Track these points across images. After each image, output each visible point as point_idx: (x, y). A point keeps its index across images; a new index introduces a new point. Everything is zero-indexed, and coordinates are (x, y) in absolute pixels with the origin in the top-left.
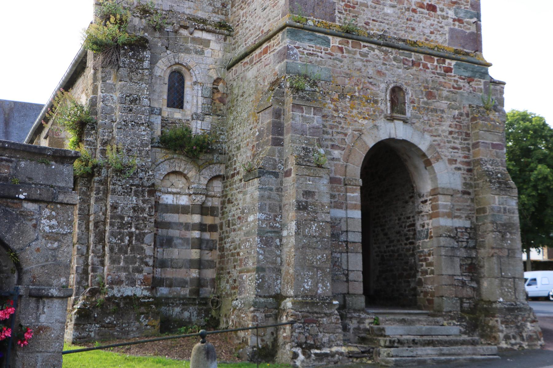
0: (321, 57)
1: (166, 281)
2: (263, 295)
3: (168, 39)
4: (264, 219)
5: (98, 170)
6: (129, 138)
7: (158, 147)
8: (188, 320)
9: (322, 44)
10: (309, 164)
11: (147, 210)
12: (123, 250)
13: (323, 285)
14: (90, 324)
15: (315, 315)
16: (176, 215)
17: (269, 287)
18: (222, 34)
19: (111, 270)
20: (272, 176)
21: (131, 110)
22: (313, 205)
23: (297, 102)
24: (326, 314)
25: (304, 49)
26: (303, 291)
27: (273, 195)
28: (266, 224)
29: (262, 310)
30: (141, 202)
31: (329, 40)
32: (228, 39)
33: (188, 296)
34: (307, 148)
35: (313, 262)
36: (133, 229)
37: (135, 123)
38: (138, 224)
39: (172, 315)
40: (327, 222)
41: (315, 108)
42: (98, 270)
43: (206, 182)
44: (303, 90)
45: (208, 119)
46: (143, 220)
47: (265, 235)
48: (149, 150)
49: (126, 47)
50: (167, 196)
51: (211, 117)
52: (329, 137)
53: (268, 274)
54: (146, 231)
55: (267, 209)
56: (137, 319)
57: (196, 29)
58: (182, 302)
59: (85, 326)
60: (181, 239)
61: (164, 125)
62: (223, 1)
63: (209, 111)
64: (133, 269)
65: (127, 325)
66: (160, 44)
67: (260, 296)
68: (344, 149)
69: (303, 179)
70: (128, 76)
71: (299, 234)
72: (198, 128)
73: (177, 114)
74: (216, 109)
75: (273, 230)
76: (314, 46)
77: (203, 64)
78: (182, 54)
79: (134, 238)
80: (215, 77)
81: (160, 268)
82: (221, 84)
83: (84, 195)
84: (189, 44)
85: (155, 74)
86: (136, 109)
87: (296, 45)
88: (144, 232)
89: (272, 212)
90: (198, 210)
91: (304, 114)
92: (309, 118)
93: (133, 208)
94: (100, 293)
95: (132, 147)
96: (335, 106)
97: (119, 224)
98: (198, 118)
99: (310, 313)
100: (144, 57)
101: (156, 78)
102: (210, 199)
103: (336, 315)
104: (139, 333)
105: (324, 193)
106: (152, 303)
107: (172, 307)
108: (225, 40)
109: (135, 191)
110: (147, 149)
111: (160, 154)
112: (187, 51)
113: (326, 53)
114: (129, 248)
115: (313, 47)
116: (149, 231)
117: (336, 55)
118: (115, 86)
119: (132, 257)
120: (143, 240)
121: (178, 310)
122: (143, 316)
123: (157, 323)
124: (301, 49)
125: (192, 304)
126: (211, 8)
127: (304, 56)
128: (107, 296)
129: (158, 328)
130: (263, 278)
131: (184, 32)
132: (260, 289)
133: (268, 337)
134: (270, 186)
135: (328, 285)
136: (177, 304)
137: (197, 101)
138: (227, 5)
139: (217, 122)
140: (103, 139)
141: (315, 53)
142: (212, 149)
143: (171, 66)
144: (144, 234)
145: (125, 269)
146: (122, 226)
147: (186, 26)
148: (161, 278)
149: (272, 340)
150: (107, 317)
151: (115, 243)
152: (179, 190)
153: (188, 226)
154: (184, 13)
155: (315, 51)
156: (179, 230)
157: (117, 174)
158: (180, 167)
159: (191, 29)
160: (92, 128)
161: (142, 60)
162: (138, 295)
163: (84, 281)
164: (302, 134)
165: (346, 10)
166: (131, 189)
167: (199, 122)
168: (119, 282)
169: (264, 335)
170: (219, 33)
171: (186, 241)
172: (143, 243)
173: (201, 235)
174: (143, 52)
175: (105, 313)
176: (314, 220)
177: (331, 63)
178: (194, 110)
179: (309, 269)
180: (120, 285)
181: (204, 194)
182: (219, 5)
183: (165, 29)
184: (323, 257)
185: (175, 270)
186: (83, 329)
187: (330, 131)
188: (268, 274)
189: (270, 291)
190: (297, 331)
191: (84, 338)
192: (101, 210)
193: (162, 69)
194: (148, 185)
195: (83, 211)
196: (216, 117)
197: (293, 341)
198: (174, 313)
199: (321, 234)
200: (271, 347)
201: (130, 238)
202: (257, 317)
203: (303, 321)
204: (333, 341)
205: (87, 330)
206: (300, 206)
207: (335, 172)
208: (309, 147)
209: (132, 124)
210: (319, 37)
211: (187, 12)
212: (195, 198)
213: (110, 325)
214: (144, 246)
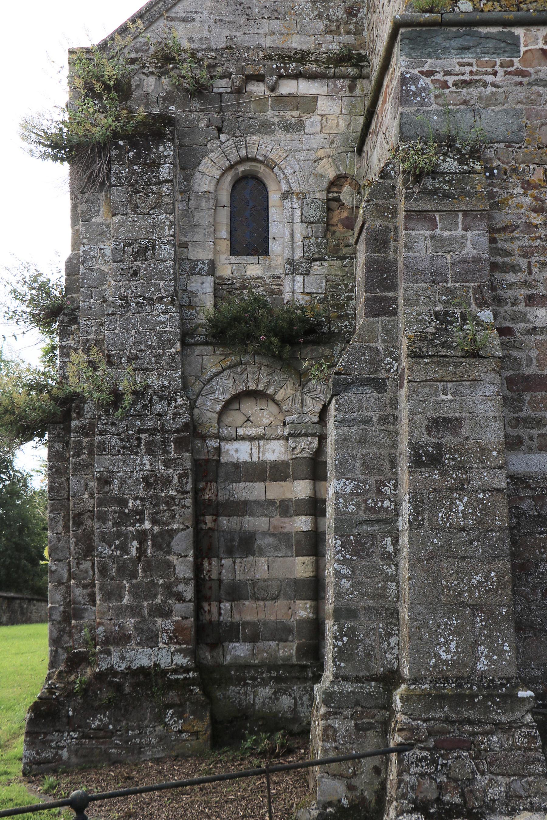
0: (494, 85)
1: (244, 629)
2: (354, 674)
3: (221, 110)
4: (352, 493)
5: (78, 407)
6: (133, 332)
7: (206, 343)
8: (289, 715)
9: (496, 51)
10: (443, 352)
11: (175, 481)
12: (126, 571)
13: (491, 649)
14: (58, 731)
15: (467, 727)
16: (259, 486)
17: (368, 655)
18: (344, 77)
19: (104, 613)
20: (368, 390)
21: (135, 274)
22: (456, 450)
23: (415, 206)
24: (498, 725)
25: (447, 73)
26: (435, 666)
27: (372, 433)
28: (357, 505)
29: (348, 712)
30: (160, 465)
31: (518, 38)
32: (358, 87)
33: (294, 660)
34: (446, 314)
35: (460, 594)
36: (147, 525)
37: (145, 298)
38: (157, 513)
39: (254, 705)
40: (498, 490)
41: (466, 213)
42: (86, 615)
44: (434, 173)
45: (318, 269)
46: (167, 504)
47: (355, 531)
48: (177, 353)
49: (121, 143)
50: (236, 445)
51: (325, 264)
52: (521, 276)
53: (363, 623)
54: (175, 526)
55: (358, 466)
56: (160, 718)
57: (281, 77)
58: (274, 674)
59: (49, 737)
60: (274, 535)
62: (348, 4)
63: (319, 252)
64: (150, 610)
65: (137, 732)
66: (202, 125)
67: (345, 679)
69: (426, 390)
70: (129, 202)
71: (420, 526)
72: (297, 290)
73: (254, 268)
74: (338, 245)
75: (374, 516)
76: (473, 61)
77: (303, 150)
78: (255, 138)
79: (149, 543)
80: (331, 174)
81: (228, 601)
82: (346, 188)
83: (58, 460)
84: (270, 113)
85: (196, 188)
86: (146, 270)
87: (426, 68)
88: (172, 530)
89: (371, 474)
90: (305, 469)
91: (438, 232)
92: (454, 240)
93: (146, 479)
94: (89, 664)
95: (140, 351)
96: (536, 198)
97: (116, 515)
99: (452, 723)
100: (160, 157)
101: (199, 197)
103: (528, 726)
104: (163, 750)
105: (486, 418)
106: (193, 681)
107: (253, 686)
108: (352, 88)
109: (148, 444)
110: (173, 350)
111: (210, 360)
112: (266, 128)
113: (506, 73)
114: (140, 565)
115: (470, 65)
116: (181, 527)
117: (537, 73)
118: (108, 226)
119: (147, 583)
120: (169, 545)
121: (265, 692)
122: (171, 711)
123: (202, 726)
124: (439, 76)
125: (298, 678)
126: (320, 25)
127: (446, 91)
128: (98, 670)
129: (205, 737)
130: (351, 633)
131: (258, 89)
132: (345, 661)
133: (364, 778)
134: (365, 413)
135: (506, 648)
136: (263, 679)
137: (292, 234)
138: (359, 11)
139: (339, 273)
140: (88, 340)
141: (477, 77)
142: (330, 332)
143: (231, 167)
144: (172, 533)
145: (134, 610)
146: (123, 519)
147: (259, 75)
148: (232, 623)
149: (377, 787)
150: (94, 716)
151: (110, 557)
152: (261, 431)
153: (288, 507)
154: (259, 47)
155: (478, 73)
156: (266, 516)
157: (107, 411)
158: (258, 381)
159: (271, 80)
160: (70, 320)
161: (155, 165)
162: (163, 666)
163: (66, 638)
164: (434, 282)
166: (139, 439)
167: (299, 278)
168: (123, 639)
169: (354, 774)
170: (335, 77)
171: (284, 538)
172: (169, 553)
174: (157, 147)
175: (90, 707)
176: (461, 487)
177: (522, 96)
178: (287, 254)
179: (452, 611)
180: (125, 645)
181: (313, 435)
182: (340, 13)
183: (215, 90)
184: (487, 577)
185: (261, 603)
186: (45, 744)
187: (523, 263)
188: (363, 623)
189: (371, 664)
190: (414, 769)
191: (47, 761)
192: (86, 489)
193: (209, 174)
194: (175, 427)
195: (58, 492)
196: (338, 263)
197: (404, 796)
198: (259, 701)
199: (480, 522)
200: (373, 804)
201: (140, 543)
202: (335, 731)
203: (432, 743)
204: (520, 797)
205: (53, 744)
206: (420, 456)
207: (538, 361)
208: (452, 310)
209: (139, 303)
210: (488, 37)
211: (267, 43)
212: (293, 445)
213: (101, 734)
214: (173, 558)
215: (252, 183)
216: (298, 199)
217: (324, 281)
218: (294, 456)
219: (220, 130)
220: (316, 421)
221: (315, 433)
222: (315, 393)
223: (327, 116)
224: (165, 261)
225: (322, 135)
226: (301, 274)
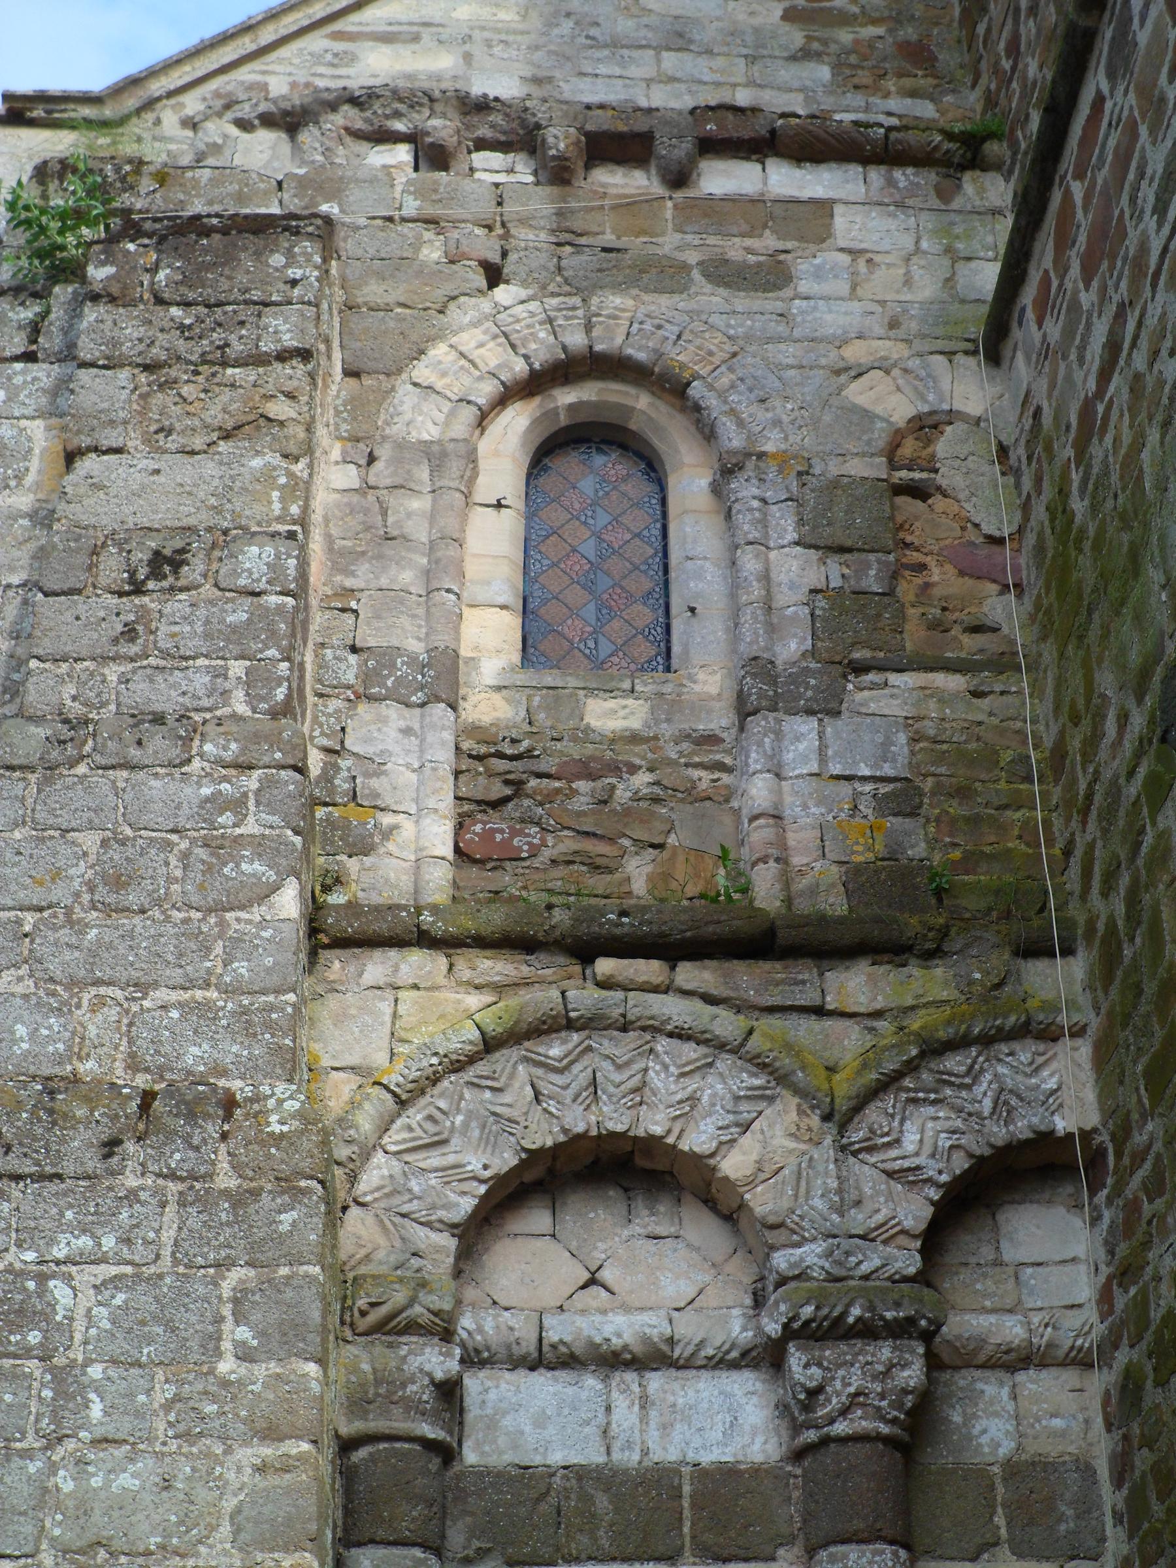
43: (915, 1211)
102: (993, 1389)
217: (902, 738)
218: (811, 1436)
219: (494, 275)
220: (912, 1270)
221: (911, 1321)
222: (893, 1153)
223: (869, 255)
224: (220, 304)
226: (810, 712)
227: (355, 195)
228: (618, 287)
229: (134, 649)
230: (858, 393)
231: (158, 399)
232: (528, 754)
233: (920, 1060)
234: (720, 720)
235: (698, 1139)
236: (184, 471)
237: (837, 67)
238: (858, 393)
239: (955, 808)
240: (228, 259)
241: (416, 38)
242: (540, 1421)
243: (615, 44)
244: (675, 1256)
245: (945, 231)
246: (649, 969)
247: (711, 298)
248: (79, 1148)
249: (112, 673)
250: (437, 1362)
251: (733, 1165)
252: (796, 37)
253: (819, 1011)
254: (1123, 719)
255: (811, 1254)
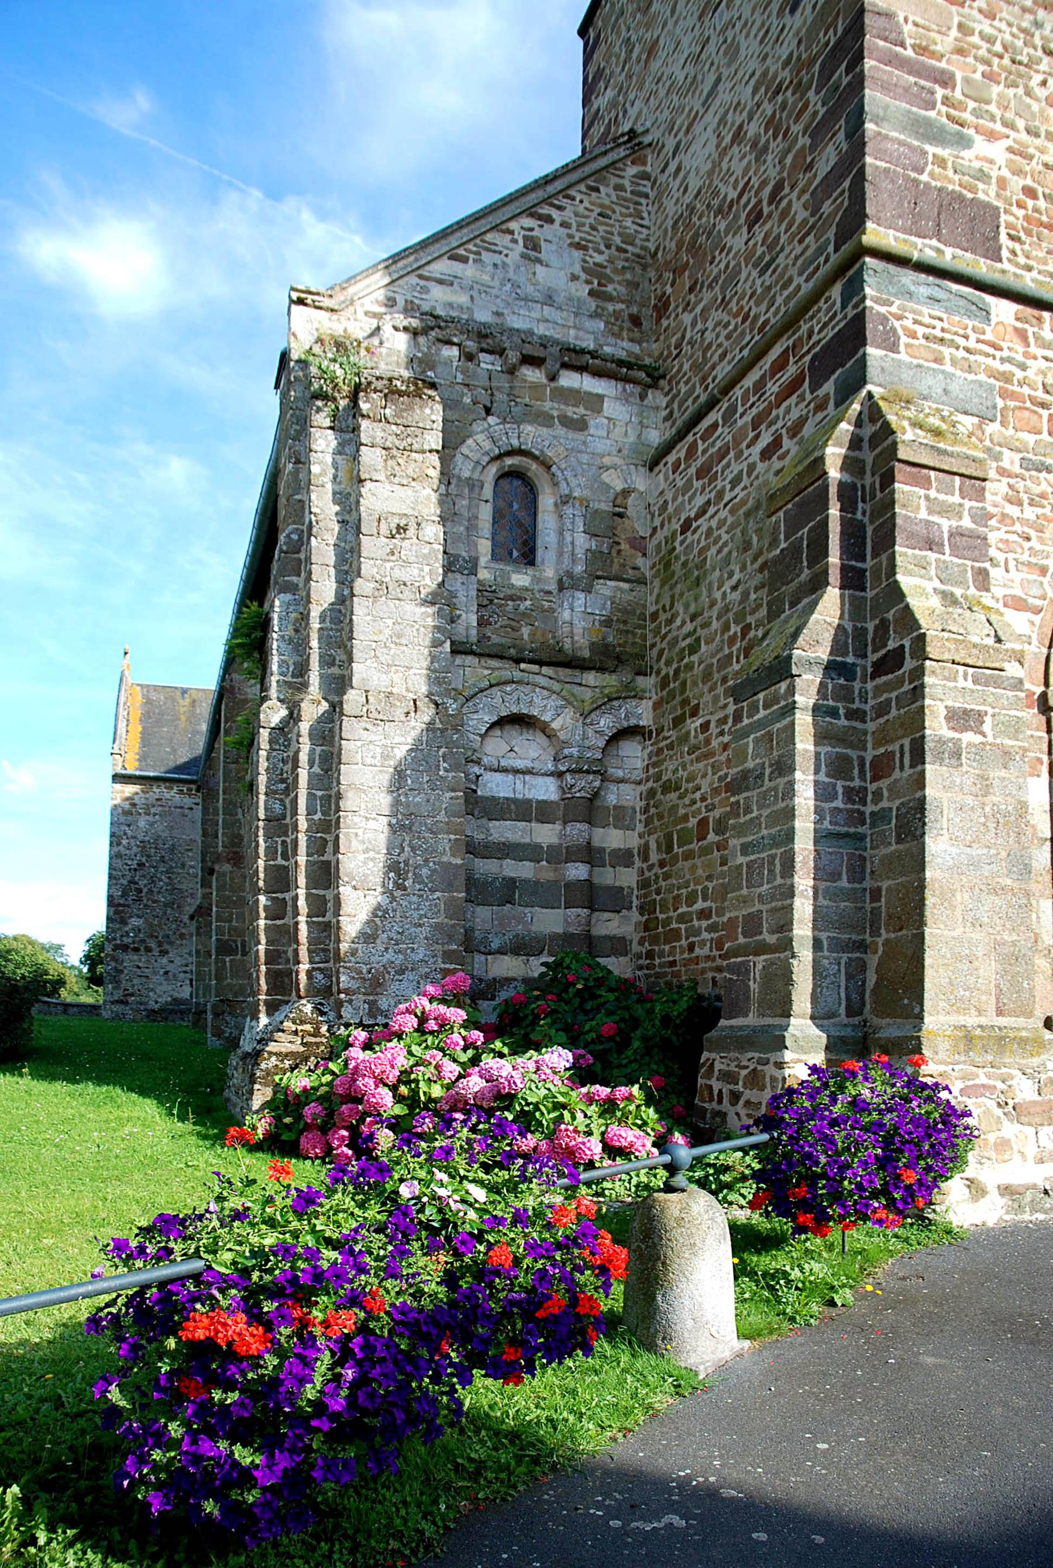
32: (650, 396)
43: (601, 743)
45: (606, 588)
61: (486, 602)
68: (1038, 611)
73: (520, 579)
76: (944, 316)
91: (933, 493)
96: (1010, 486)
98: (574, 587)
102: (613, 787)
108: (642, 397)
115: (941, 319)
131: (532, 375)
141: (947, 336)
143: (499, 457)
159: (551, 364)
165: (1028, 233)
170: (626, 380)
173: (591, 872)
215: (517, 483)
216: (581, 505)
219: (488, 411)
225: (608, 442)
227: (439, 370)
228: (530, 422)
229: (393, 558)
230: (606, 477)
231: (390, 462)
232: (494, 591)
233: (607, 701)
234: (553, 587)
235: (546, 717)
236: (401, 492)
237: (607, 323)
238: (606, 477)
239: (621, 626)
240: (410, 408)
241: (452, 284)
242: (497, 785)
243: (526, 299)
244: (534, 745)
245: (640, 414)
246: (535, 668)
247: (560, 431)
248: (399, 714)
249: (388, 565)
250: (476, 770)
251: (555, 725)
252: (592, 304)
253: (580, 684)
254: (684, 623)
255: (574, 751)
